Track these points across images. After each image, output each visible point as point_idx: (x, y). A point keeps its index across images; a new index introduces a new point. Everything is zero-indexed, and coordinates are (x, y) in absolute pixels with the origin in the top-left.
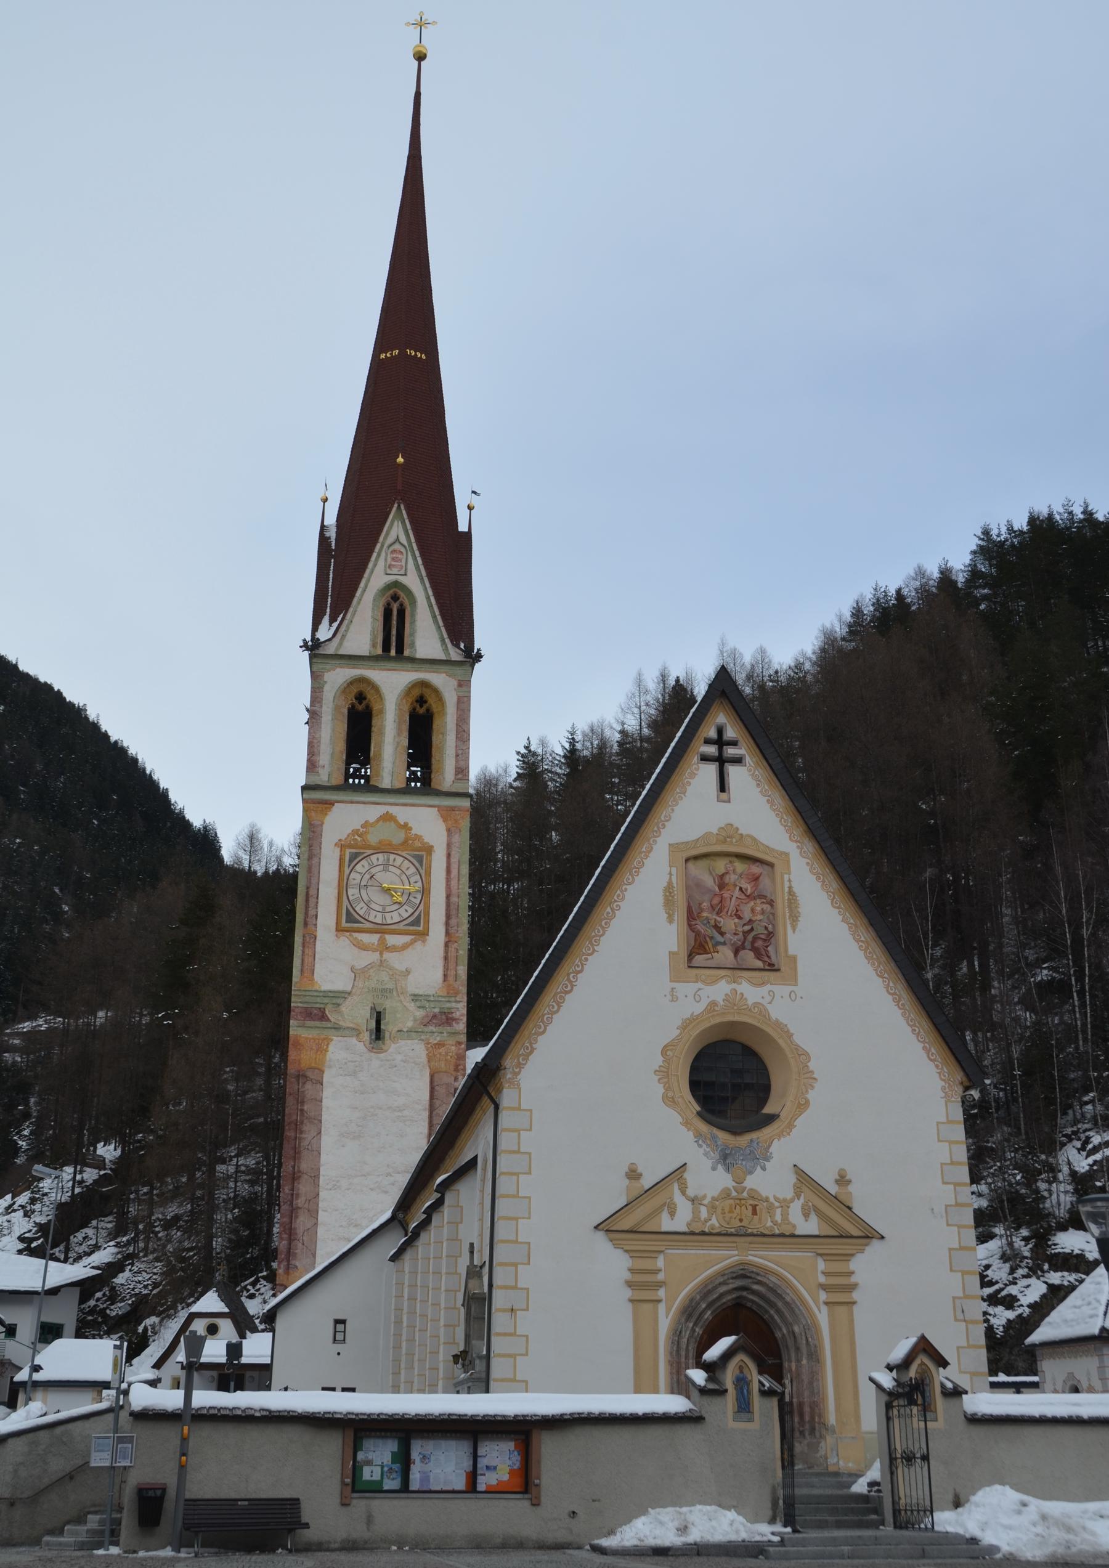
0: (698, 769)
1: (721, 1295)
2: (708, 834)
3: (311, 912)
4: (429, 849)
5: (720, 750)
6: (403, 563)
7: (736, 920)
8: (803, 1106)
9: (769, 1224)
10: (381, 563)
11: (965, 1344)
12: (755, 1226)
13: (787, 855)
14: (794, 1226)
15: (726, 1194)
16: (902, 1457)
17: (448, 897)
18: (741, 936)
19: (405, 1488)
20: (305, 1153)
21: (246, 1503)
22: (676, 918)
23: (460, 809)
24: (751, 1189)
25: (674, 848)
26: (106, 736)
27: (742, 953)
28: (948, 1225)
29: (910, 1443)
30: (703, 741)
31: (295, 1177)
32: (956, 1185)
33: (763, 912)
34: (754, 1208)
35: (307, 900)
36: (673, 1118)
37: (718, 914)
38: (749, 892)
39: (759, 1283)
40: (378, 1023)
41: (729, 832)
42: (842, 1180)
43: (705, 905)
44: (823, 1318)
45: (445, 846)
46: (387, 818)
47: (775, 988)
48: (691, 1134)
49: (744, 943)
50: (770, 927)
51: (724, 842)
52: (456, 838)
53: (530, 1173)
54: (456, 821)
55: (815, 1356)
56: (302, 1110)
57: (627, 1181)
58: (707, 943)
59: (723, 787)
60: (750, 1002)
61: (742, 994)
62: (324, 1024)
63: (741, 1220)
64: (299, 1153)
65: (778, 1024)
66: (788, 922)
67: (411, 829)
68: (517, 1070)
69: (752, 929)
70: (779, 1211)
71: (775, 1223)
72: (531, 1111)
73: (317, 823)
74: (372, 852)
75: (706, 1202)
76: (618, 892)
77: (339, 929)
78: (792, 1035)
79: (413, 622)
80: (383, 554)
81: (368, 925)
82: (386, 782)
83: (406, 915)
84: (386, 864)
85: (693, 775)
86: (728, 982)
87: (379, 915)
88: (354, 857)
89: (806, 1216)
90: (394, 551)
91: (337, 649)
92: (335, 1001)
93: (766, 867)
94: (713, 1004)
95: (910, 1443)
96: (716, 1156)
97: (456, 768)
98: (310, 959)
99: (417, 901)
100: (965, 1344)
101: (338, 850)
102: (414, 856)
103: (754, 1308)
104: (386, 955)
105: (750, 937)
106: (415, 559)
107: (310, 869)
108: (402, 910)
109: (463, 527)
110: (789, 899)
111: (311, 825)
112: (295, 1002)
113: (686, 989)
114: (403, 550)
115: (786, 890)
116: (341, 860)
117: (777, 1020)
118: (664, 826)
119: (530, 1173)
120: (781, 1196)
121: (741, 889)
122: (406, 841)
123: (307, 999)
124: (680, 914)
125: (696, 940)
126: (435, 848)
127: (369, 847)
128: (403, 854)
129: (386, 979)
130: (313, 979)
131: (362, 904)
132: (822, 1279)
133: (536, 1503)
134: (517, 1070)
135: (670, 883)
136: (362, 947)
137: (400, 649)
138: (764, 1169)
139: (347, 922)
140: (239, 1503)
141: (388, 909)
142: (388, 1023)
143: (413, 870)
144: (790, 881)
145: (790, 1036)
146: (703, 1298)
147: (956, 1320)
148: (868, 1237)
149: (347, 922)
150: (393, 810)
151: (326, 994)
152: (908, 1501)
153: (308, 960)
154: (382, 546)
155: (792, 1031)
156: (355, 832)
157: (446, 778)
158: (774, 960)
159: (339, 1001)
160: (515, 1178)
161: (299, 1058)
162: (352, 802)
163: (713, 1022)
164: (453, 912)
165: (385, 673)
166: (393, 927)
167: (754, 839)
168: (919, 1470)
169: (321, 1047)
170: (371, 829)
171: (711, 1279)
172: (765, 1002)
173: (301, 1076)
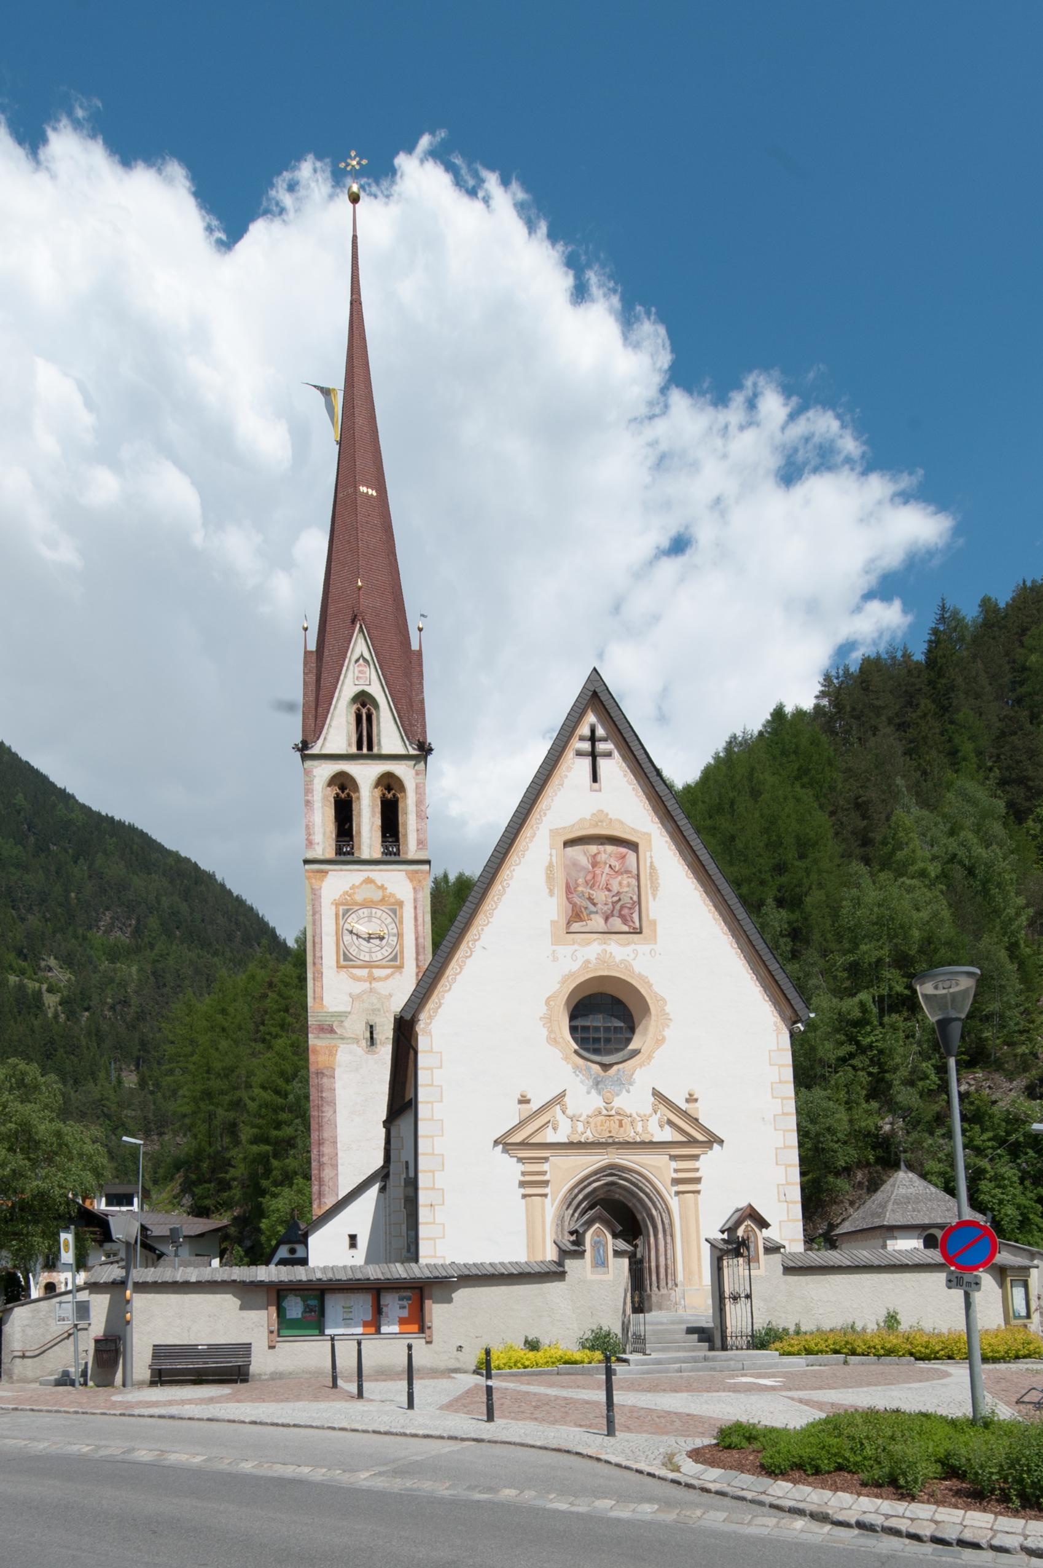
0: (573, 764)
2: (582, 820)
3: (318, 954)
4: (400, 904)
5: (593, 746)
7: (607, 893)
8: (660, 1041)
9: (632, 1134)
10: (350, 675)
11: (786, 1219)
13: (649, 835)
16: (730, 1298)
17: (417, 939)
18: (610, 906)
20: (326, 1127)
21: (205, 1347)
22: (556, 892)
25: (554, 833)
26: (230, 892)
27: (611, 920)
28: (776, 1130)
29: (737, 1286)
30: (577, 738)
31: (320, 1143)
32: (783, 1098)
33: (629, 885)
34: (620, 1121)
35: (314, 946)
36: (555, 1054)
37: (591, 888)
38: (617, 869)
40: (371, 1033)
41: (600, 816)
42: (691, 1099)
43: (581, 881)
44: (674, 1203)
45: (412, 901)
46: (369, 881)
47: (638, 947)
48: (570, 1066)
49: (612, 911)
51: (597, 825)
52: (420, 895)
53: (441, 1101)
55: (669, 1232)
56: (322, 1097)
58: (582, 912)
60: (618, 960)
61: (611, 953)
62: (333, 1036)
65: (640, 976)
67: (386, 889)
68: (429, 1021)
69: (620, 900)
70: (640, 1124)
73: (316, 887)
76: (508, 872)
77: (339, 967)
78: (652, 985)
80: (351, 667)
81: (359, 963)
82: (365, 854)
83: (386, 954)
84: (370, 917)
85: (569, 769)
86: (599, 944)
87: (367, 955)
88: (346, 912)
92: (339, 1019)
94: (588, 962)
95: (737, 1286)
96: (591, 1083)
99: (395, 943)
100: (786, 1219)
101: (334, 907)
104: (375, 985)
105: (618, 907)
108: (383, 951)
109: (415, 646)
110: (650, 873)
112: (311, 1021)
113: (564, 951)
115: (648, 864)
116: (337, 915)
117: (640, 974)
118: (545, 814)
119: (441, 1101)
120: (642, 1113)
121: (610, 866)
123: (319, 1018)
125: (573, 910)
126: (405, 903)
127: (356, 904)
128: (383, 908)
129: (375, 1001)
130: (322, 1004)
131: (354, 947)
134: (429, 1021)
136: (358, 979)
137: (370, 748)
138: (628, 1091)
139: (344, 960)
140: (200, 1347)
141: (373, 950)
142: (378, 1034)
143: (389, 920)
144: (651, 857)
145: (650, 986)
147: (779, 1201)
148: (692, 1142)
149: (344, 960)
150: (373, 875)
151: (333, 1015)
152: (734, 1330)
153: (318, 990)
154: (350, 661)
155: (652, 981)
159: (343, 1019)
160: (430, 1105)
161: (317, 1061)
163: (588, 976)
164: (421, 950)
165: (359, 767)
166: (377, 963)
167: (621, 823)
168: (743, 1306)
169: (332, 1052)
170: (357, 890)
173: (319, 1073)
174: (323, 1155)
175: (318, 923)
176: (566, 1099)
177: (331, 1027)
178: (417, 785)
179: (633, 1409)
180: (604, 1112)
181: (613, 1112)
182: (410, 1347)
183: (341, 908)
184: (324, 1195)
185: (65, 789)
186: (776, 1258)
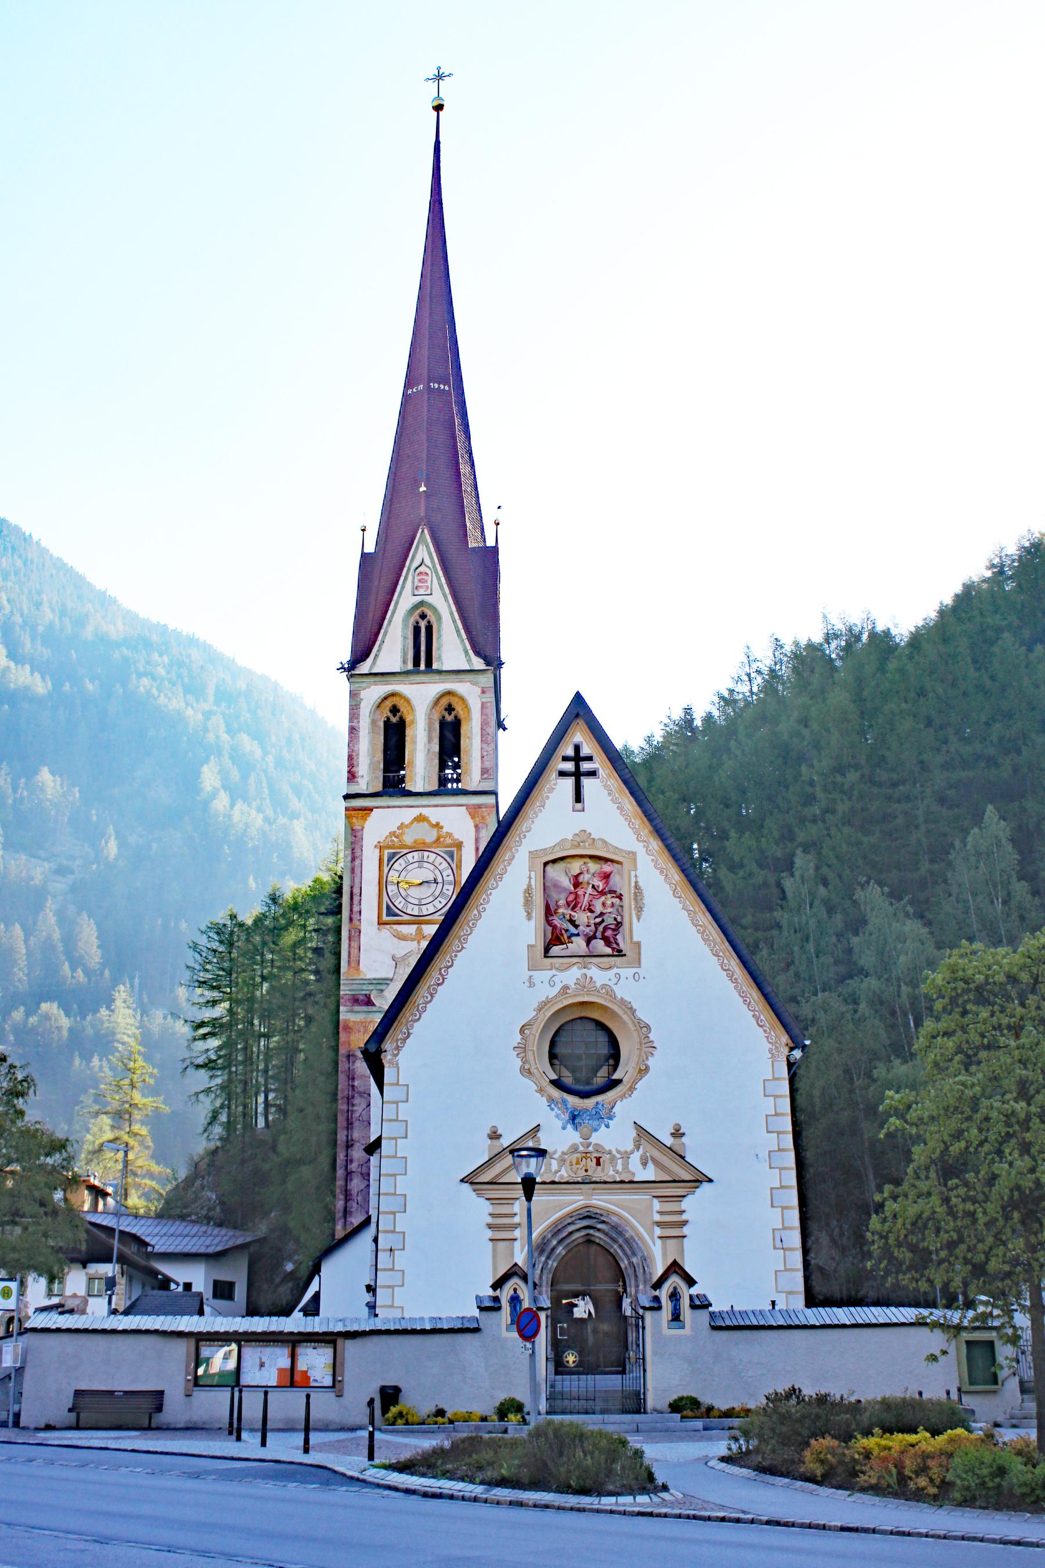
0: (555, 784)
1: (571, 1233)
3: (356, 909)
4: (459, 845)
5: (577, 766)
6: (429, 584)
9: (611, 1173)
12: (598, 1174)
14: (633, 1174)
15: (574, 1149)
18: (593, 927)
19: (197, 1382)
22: (534, 915)
23: (486, 806)
24: (596, 1144)
25: (533, 855)
27: (594, 942)
33: (613, 905)
34: (598, 1160)
35: (352, 899)
37: (573, 909)
39: (603, 1222)
41: (583, 837)
42: (677, 1134)
46: (421, 819)
48: (544, 1099)
50: (619, 919)
51: (578, 846)
54: (483, 818)
56: (353, 1086)
57: (489, 1141)
59: (578, 798)
61: (591, 978)
62: (371, 1008)
63: (586, 1171)
64: (352, 1123)
66: (634, 913)
67: (442, 828)
69: (603, 921)
70: (620, 1162)
71: (617, 1172)
72: (407, 1086)
73: (358, 828)
74: (407, 851)
75: (556, 1156)
79: (439, 637)
81: (406, 918)
82: (418, 788)
83: (439, 906)
86: (579, 968)
88: (391, 856)
89: (645, 1164)
90: (420, 574)
91: (371, 668)
92: (379, 987)
93: (616, 865)
94: (566, 988)
96: (567, 1117)
97: (482, 769)
98: (356, 951)
102: (446, 852)
103: (602, 1243)
105: (601, 928)
106: (439, 579)
107: (353, 871)
108: (436, 903)
111: (353, 830)
114: (428, 571)
115: (633, 884)
116: (381, 860)
117: (622, 999)
118: (525, 836)
119: (406, 1137)
120: (622, 1150)
121: (593, 886)
122: (438, 839)
124: (539, 911)
131: (401, 899)
132: (657, 1218)
133: (339, 1396)
135: (529, 885)
137: (429, 663)
138: (607, 1126)
143: (445, 864)
144: (636, 876)
146: (555, 1234)
147: (775, 1248)
148: (697, 1181)
150: (425, 812)
151: (371, 982)
153: (354, 952)
154: (409, 569)
156: (393, 834)
157: (473, 779)
158: (622, 946)
162: (389, 807)
171: (561, 1219)
172: (611, 984)
174: (351, 1161)
175: (357, 871)
176: (539, 1134)
177: (368, 997)
178: (483, 704)
179: (382, 1441)
180: (581, 1149)
181: (591, 1149)
182: (308, 1396)
183: (386, 852)
184: (351, 1213)
185: (104, 593)
186: (703, 1316)
